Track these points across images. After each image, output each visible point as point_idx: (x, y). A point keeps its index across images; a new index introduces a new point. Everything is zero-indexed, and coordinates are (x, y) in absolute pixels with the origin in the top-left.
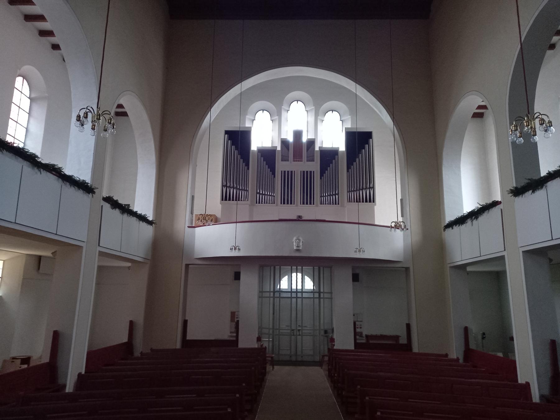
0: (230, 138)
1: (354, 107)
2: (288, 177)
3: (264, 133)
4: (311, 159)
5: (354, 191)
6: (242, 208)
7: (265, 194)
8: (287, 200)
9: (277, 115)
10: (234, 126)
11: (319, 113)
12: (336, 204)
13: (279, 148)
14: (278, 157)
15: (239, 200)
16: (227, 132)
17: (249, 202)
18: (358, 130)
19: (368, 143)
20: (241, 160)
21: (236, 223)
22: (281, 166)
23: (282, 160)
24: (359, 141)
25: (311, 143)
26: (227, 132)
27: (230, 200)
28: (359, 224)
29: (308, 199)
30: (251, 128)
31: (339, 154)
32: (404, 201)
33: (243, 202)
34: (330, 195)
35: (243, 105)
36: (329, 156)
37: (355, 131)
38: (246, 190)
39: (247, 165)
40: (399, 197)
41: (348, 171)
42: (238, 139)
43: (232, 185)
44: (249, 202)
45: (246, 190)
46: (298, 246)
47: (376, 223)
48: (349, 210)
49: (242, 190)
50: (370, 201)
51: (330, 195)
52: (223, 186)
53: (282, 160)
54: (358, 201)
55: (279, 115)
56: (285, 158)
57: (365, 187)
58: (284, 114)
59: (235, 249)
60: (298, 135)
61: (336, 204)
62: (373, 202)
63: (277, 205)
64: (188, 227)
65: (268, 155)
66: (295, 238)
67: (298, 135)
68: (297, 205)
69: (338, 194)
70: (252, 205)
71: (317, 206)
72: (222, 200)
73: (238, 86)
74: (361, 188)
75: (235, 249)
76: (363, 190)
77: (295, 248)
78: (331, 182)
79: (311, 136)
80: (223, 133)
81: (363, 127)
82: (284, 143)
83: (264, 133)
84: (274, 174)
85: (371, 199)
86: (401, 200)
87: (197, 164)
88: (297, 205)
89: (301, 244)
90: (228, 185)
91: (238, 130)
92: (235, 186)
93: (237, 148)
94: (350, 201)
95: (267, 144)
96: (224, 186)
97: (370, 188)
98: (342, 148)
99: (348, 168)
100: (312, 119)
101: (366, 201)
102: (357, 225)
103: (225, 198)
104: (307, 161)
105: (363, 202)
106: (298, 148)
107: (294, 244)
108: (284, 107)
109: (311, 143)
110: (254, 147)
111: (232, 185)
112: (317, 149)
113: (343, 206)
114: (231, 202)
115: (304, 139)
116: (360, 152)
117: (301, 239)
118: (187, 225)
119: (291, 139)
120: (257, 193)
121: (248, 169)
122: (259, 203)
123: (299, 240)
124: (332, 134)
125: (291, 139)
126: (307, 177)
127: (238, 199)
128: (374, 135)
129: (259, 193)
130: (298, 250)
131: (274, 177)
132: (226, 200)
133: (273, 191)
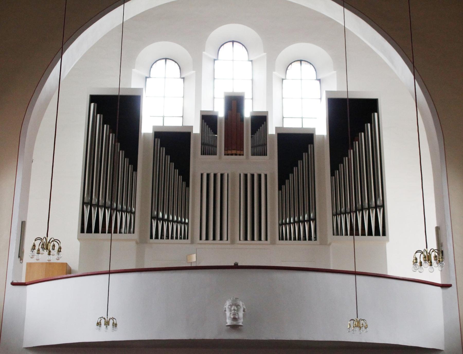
0: (99, 110)
1: (344, 51)
2: (215, 183)
3: (167, 105)
4: (260, 149)
5: (345, 213)
6: (123, 248)
7: (168, 220)
8: (214, 231)
9: (191, 69)
10: (108, 86)
11: (275, 66)
12: (310, 239)
13: (197, 130)
14: (195, 147)
15: (115, 232)
16: (93, 99)
17: (135, 236)
18: (350, 97)
19: (370, 120)
20: (122, 154)
21: (109, 273)
22: (200, 164)
23: (203, 153)
24: (353, 117)
25: (260, 121)
26: (93, 99)
27: (97, 231)
28: (355, 273)
29: (253, 230)
30: (141, 90)
31: (316, 141)
32: (442, 232)
33: (123, 236)
34: (299, 221)
35: (126, 43)
36: (295, 145)
37: (345, 97)
38: (131, 212)
39: (134, 162)
40: (432, 223)
41: (333, 174)
42: (115, 113)
43: (101, 202)
44: (135, 236)
45: (131, 212)
46: (235, 319)
47: (390, 273)
48: (340, 250)
49: (122, 211)
50: (377, 234)
51: (299, 221)
52: (84, 203)
53: (203, 153)
54: (354, 232)
55: (197, 65)
56: (208, 149)
57: (366, 206)
58: (206, 67)
59: (107, 323)
60: (234, 103)
61: (310, 239)
62: (384, 234)
63: (192, 242)
64: (13, 284)
65: (174, 143)
66: (228, 303)
67: (234, 103)
68: (233, 242)
69: (315, 220)
70: (141, 242)
71: (273, 243)
72: (82, 231)
73: (118, 11)
74: (359, 206)
75: (107, 323)
76: (363, 209)
77: (229, 322)
78: (301, 201)
79: (260, 108)
80: (87, 99)
81: (360, 90)
82: (208, 120)
83: (167, 105)
84: (186, 179)
85: (380, 230)
86: (438, 229)
87: (34, 157)
88: (220, 158)
89: (241, 314)
90: (94, 201)
91: (116, 93)
92: (108, 203)
93: (112, 130)
94: (337, 232)
95: (173, 122)
96: (87, 204)
97: (376, 207)
98: (321, 129)
99: (334, 167)
100: (261, 75)
101: (370, 234)
102: (353, 277)
103: (88, 227)
104: (253, 154)
105: (363, 234)
106: (234, 129)
107: (228, 313)
108: (208, 54)
109: (260, 121)
110: (147, 127)
111: (101, 202)
112: (272, 131)
113: (324, 243)
114: (100, 235)
115: (247, 113)
116: (355, 137)
117: (241, 303)
118: (9, 281)
119: (220, 112)
120: (152, 218)
121: (135, 169)
122: (157, 237)
123: (237, 306)
124: (300, 105)
125: (220, 112)
126: (252, 185)
127: (113, 229)
128: (382, 106)
129: (157, 218)
130: (235, 327)
131: (188, 185)
132: (89, 231)
133: (186, 215)
